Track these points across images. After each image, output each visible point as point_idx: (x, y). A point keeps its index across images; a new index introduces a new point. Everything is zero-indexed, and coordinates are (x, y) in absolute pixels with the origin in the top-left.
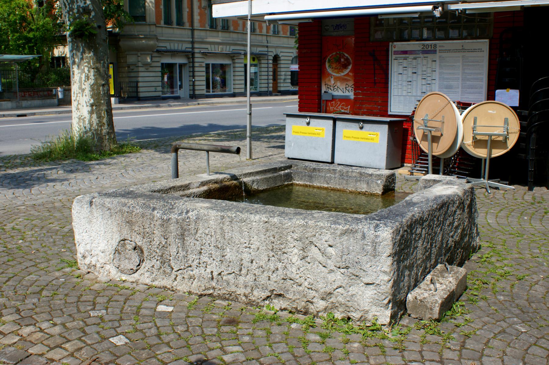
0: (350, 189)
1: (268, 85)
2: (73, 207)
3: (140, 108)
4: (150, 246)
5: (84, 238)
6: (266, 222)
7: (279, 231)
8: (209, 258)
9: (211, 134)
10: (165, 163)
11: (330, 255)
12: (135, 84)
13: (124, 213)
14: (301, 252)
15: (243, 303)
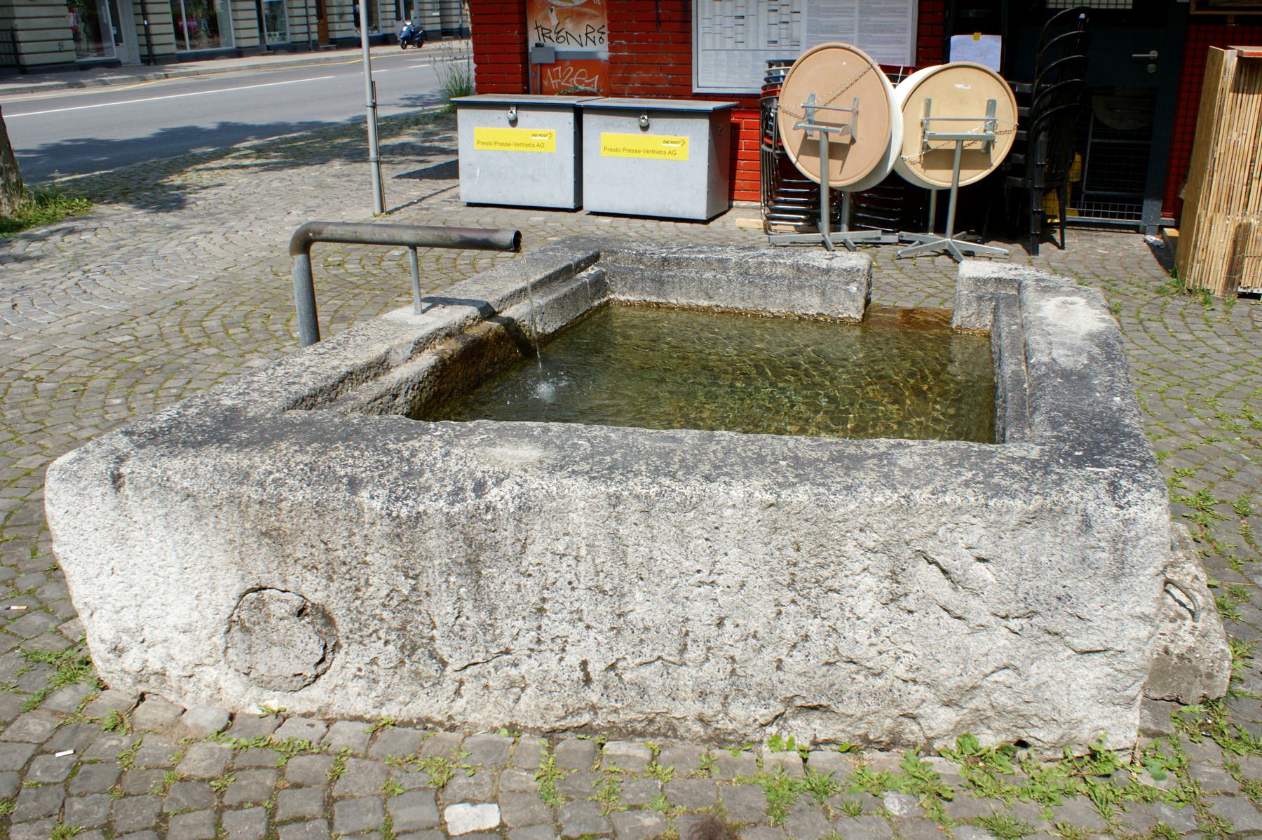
0: (774, 310)
1: (309, 29)
2: (48, 494)
3: (32, 90)
4: (358, 603)
5: (106, 592)
6: (771, 505)
7: (815, 529)
8: (572, 623)
9: (238, 150)
10: (176, 242)
11: (981, 584)
12: (9, 35)
13: (247, 507)
14: (887, 583)
15: (692, 740)
